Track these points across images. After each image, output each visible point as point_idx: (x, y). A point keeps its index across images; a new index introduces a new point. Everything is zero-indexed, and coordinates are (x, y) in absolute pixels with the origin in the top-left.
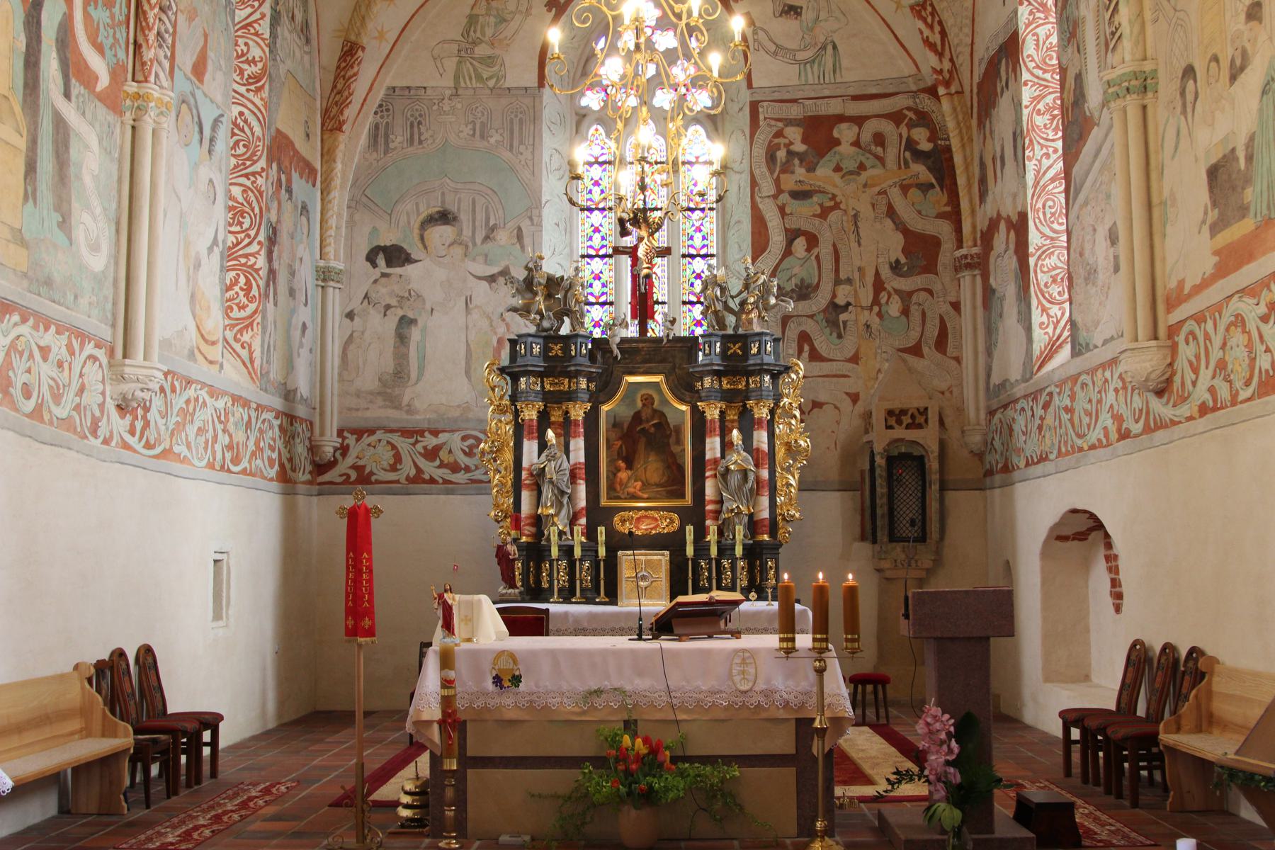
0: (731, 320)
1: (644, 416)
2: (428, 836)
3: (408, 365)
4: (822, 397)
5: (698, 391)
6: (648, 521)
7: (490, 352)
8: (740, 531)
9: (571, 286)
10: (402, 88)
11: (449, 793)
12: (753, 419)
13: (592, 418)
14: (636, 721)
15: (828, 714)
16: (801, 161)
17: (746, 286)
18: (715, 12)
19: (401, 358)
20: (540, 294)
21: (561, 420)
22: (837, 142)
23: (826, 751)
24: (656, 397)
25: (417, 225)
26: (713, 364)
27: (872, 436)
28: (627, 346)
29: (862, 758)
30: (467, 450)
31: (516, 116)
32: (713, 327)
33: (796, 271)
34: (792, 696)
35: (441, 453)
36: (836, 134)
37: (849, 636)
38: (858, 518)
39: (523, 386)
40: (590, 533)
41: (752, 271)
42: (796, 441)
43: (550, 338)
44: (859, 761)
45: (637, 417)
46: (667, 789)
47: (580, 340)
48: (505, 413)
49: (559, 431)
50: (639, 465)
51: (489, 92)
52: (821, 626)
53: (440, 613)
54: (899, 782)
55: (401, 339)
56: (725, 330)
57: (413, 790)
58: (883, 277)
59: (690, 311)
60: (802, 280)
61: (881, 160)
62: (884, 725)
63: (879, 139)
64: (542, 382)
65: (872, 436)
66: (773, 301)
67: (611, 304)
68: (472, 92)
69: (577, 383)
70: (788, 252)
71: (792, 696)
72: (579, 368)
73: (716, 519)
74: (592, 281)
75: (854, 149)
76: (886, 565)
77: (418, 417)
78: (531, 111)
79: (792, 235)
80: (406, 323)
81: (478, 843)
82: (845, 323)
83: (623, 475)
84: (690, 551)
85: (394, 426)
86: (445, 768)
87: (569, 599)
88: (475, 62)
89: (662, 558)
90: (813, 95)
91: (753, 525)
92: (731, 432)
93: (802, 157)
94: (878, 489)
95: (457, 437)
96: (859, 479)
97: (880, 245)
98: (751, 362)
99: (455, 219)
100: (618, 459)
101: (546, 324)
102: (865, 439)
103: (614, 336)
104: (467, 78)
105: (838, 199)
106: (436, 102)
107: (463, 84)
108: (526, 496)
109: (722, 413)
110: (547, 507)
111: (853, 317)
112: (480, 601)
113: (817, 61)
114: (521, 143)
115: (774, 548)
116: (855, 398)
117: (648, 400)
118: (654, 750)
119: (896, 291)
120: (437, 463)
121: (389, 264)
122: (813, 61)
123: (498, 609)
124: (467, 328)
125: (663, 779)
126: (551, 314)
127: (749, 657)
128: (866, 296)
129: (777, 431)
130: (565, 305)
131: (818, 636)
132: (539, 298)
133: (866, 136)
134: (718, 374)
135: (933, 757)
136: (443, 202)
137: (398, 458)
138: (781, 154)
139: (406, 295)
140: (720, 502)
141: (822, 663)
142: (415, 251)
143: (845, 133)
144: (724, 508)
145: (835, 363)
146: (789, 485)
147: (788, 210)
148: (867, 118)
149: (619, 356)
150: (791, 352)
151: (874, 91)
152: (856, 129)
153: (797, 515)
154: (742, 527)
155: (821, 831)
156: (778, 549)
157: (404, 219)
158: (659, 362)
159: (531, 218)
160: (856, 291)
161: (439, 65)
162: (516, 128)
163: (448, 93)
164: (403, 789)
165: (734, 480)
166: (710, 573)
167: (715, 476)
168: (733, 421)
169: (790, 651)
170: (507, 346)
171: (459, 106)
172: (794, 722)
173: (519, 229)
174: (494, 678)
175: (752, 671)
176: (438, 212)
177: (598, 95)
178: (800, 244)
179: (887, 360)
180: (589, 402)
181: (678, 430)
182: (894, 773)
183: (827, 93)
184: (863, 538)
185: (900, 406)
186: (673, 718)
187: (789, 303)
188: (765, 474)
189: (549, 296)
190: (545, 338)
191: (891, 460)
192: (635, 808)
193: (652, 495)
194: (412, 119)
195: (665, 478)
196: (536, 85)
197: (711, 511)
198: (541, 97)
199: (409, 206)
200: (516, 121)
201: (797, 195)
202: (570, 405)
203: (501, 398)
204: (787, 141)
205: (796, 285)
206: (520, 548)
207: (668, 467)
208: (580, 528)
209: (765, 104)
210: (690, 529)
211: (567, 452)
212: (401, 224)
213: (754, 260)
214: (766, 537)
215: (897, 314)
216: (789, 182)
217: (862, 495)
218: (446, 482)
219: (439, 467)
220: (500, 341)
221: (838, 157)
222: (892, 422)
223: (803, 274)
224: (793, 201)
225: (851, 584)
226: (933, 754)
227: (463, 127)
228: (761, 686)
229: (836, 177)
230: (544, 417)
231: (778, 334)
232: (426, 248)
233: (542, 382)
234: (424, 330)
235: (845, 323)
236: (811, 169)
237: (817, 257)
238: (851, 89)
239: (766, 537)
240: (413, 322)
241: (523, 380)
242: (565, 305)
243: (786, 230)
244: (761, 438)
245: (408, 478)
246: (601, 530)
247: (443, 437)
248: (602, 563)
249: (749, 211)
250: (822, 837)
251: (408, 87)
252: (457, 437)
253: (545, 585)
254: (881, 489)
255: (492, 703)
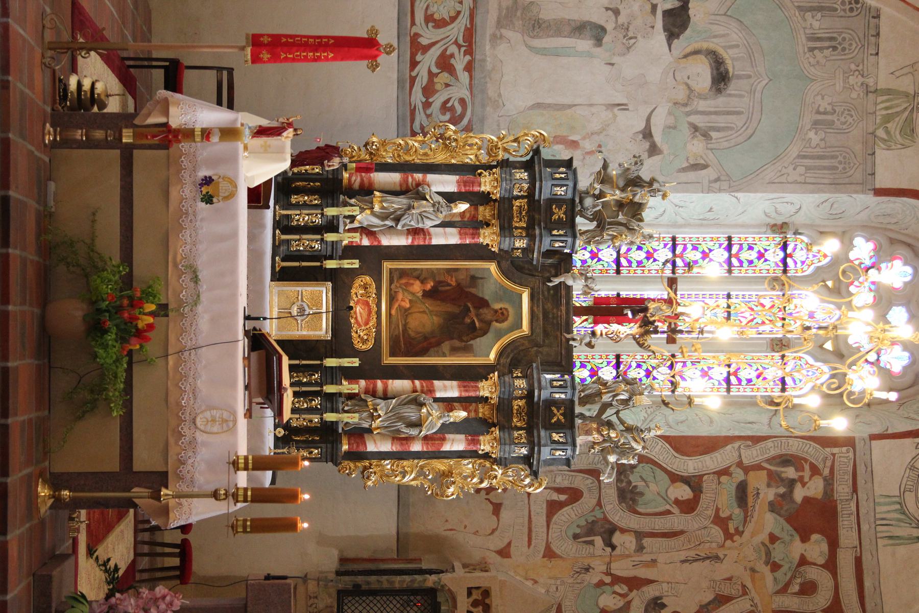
0: (591, 410)
1: (484, 311)
2: (53, 110)
3: (548, 36)
4: (504, 514)
5: (511, 372)
6: (365, 316)
7: (562, 132)
8: (353, 419)
9: (631, 230)
10: (878, 27)
11: (99, 134)
12: (479, 434)
13: (482, 253)
14: (167, 316)
15: (172, 502)
16: (782, 496)
17: (629, 429)
18: (853, 402)
19: (557, 28)
20: (623, 195)
21: (480, 218)
22: (805, 539)
23: (135, 500)
24: (504, 325)
25: (712, 46)
26: (540, 390)
27: (460, 571)
28: (563, 293)
29: (107, 547)
30: (449, 105)
31: (840, 163)
32: (583, 391)
33: (653, 487)
34: (189, 467)
35: (445, 75)
36: (815, 537)
37: (248, 523)
38: (365, 555)
39: (518, 176)
40: (351, 251)
41: (647, 435)
42: (454, 483)
43: (572, 207)
44: (105, 544)
45: (483, 303)
46: (105, 347)
47: (570, 240)
48: (489, 154)
49: (468, 215)
50: (429, 305)
51: (871, 130)
52: (259, 496)
53: (275, 124)
54: (106, 571)
55: (580, 28)
56: (579, 404)
57: (96, 91)
58: (645, 589)
59: (609, 363)
60: (642, 494)
61: (783, 590)
62: (134, 577)
63: (808, 589)
64: (522, 197)
65: (460, 571)
66: (612, 458)
67: (618, 272)
68: (871, 109)
69: (521, 237)
70: (675, 478)
71: (189, 467)
72: (537, 239)
73: (367, 392)
74: (645, 250)
75: (797, 557)
76: (312, 586)
77: (488, 47)
78: (847, 181)
79: (694, 483)
80: (598, 33)
81: (47, 160)
82: (591, 543)
83: (417, 287)
84: (331, 362)
85: (478, 20)
86: (124, 130)
87: (278, 228)
88: (906, 113)
89: (323, 330)
90: (862, 511)
91: (359, 434)
92: (464, 410)
93: (788, 496)
94: (398, 578)
95: (465, 93)
96: (411, 556)
97: (682, 586)
98: (543, 433)
99: (719, 91)
100: (434, 281)
101: (588, 202)
102: (457, 565)
103: (574, 278)
104: (888, 104)
105: (736, 538)
106: (860, 68)
107: (880, 99)
108: (393, 178)
109: (485, 400)
110: (381, 202)
111: (599, 552)
112: (285, 160)
113: (903, 517)
114: (808, 168)
115: (333, 457)
116: (504, 553)
117: (501, 316)
118: (140, 334)
119: (629, 603)
120: (435, 70)
121: (667, 14)
122: (904, 513)
123: (272, 179)
124: (591, 105)
125: (115, 344)
126: (600, 208)
127: (228, 426)
128: (622, 568)
129: (466, 462)
130: (610, 224)
131: (249, 493)
132: (618, 195)
133: (813, 574)
134: (529, 396)
135: (132, 601)
136: (739, 77)
137: (441, 24)
138: (790, 472)
139: (630, 34)
140: (386, 397)
141: (223, 497)
142: (682, 44)
143: (817, 548)
144: (378, 401)
145: (545, 529)
146: (404, 474)
147: (724, 479)
148: (834, 574)
149: (550, 284)
150: (559, 480)
151: (867, 584)
152: (821, 561)
153: (370, 483)
154: (356, 420)
155: (60, 495)
156: (332, 461)
157: (721, 30)
158: (544, 327)
159: (717, 180)
160: (628, 556)
161: (905, 71)
162: (826, 163)
163: (871, 81)
164: (96, 81)
165: (411, 413)
166: (306, 384)
167: (415, 391)
168: (476, 411)
169: (235, 465)
170: (565, 156)
171: (854, 95)
172: (165, 470)
173: (705, 167)
174: (210, 177)
175: (215, 429)
176: (727, 72)
177: (868, 258)
178: (684, 492)
179: (548, 591)
180: (500, 250)
181: (467, 350)
182: (116, 565)
183: (865, 527)
184: (343, 560)
185: (494, 605)
186: (170, 351)
187: (609, 477)
188: (417, 447)
189: (620, 205)
190: (573, 200)
191: (431, 593)
192: (85, 316)
193: (394, 319)
194: (840, 39)
195: (412, 334)
196: (878, 186)
197: (375, 386)
198: (863, 192)
199: (735, 36)
200: (834, 162)
201: (742, 492)
202: (496, 229)
203: (505, 150)
204: (806, 479)
205: (635, 487)
206: (337, 172)
207: (426, 338)
208: (358, 240)
209: (851, 455)
210: (355, 362)
211: (444, 225)
212: (714, 27)
213: (665, 438)
214: (345, 447)
215: (601, 606)
216: (757, 481)
217: (393, 560)
218: (413, 80)
219: (430, 72)
220: (574, 144)
221: (787, 538)
222: (476, 595)
223: (648, 496)
224: (735, 485)
225: (299, 525)
226: (136, 601)
227: (828, 99)
228: (200, 437)
229: (764, 537)
230: (484, 199)
231: (576, 464)
232: (686, 56)
233: (522, 197)
234: (591, 56)
235: (591, 543)
236: (773, 507)
237: (668, 512)
238: (870, 557)
239: (345, 447)
240: (599, 41)
241: (525, 175)
242: (610, 224)
243: (701, 476)
244: (456, 443)
245: (417, 35)
246: (355, 264)
247: (464, 77)
248: (318, 264)
249: (723, 434)
250: (54, 497)
251: (878, 34)
252: (465, 93)
253: (294, 199)
254: (399, 582)
255: (186, 175)
